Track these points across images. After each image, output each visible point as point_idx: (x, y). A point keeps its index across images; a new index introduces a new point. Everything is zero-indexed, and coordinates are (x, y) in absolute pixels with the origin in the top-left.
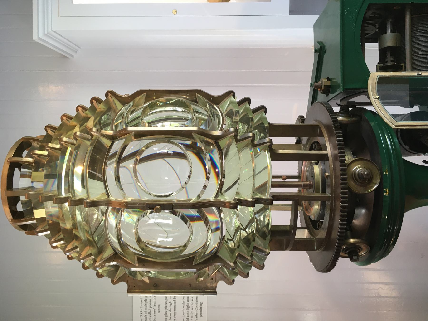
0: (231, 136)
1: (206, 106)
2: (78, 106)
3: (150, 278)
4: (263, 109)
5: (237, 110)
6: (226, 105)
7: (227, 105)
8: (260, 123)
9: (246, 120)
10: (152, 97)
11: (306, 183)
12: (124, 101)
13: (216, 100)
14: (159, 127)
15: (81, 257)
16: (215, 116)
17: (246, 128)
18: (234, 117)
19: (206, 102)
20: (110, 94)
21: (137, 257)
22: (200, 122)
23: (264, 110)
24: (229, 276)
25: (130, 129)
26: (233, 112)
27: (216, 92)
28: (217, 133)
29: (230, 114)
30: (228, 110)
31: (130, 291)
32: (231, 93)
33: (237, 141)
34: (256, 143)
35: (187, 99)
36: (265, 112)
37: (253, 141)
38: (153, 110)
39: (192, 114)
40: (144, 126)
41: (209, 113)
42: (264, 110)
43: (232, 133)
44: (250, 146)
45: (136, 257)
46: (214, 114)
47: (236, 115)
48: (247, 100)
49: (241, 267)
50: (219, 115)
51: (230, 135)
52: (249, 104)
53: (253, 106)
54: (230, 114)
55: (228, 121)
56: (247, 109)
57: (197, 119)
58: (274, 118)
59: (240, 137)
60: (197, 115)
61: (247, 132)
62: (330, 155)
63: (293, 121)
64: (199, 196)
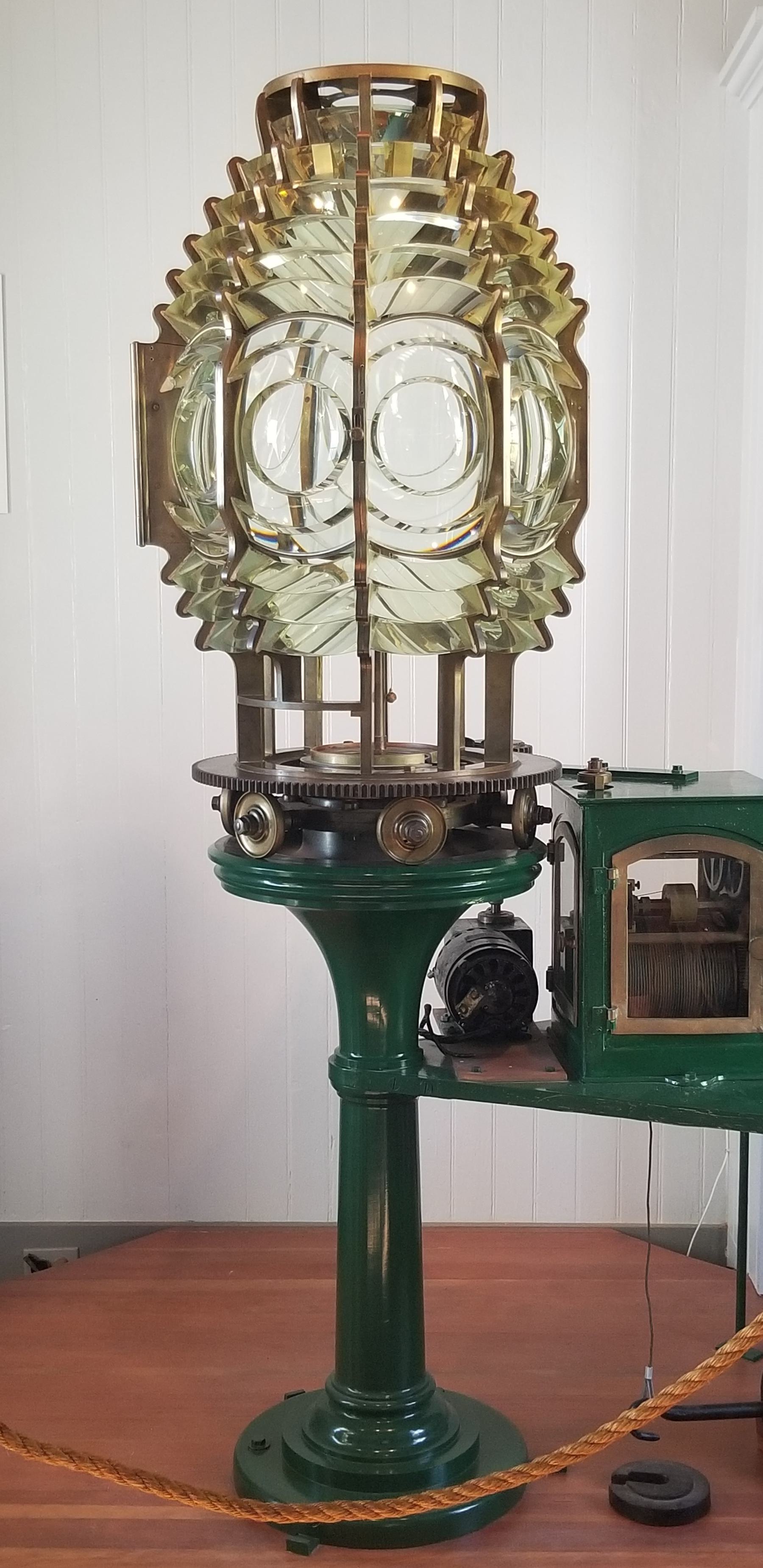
0: (490, 573)
1: (552, 521)
2: (555, 234)
3: (176, 392)
4: (547, 642)
5: (544, 586)
6: (555, 563)
7: (555, 567)
8: (516, 638)
9: (524, 604)
10: (574, 401)
11: (383, 744)
12: (567, 338)
13: (565, 544)
14: (510, 418)
15: (238, 258)
16: (531, 541)
17: (509, 605)
18: (530, 580)
19: (560, 522)
20: (580, 307)
21: (241, 380)
22: (519, 509)
23: (544, 645)
24: (182, 573)
25: (507, 368)
26: (540, 578)
27: (582, 543)
28: (497, 546)
29: (535, 571)
30: (543, 569)
31: (141, 348)
32: (579, 574)
33: (481, 586)
34: (475, 624)
35: (569, 477)
36: (539, 649)
37: (481, 617)
38: (545, 405)
39: (535, 492)
40: (515, 391)
41: (537, 529)
42: (544, 645)
43: (499, 575)
44: (466, 613)
45: (241, 376)
46: (535, 539)
47: (533, 584)
48: (565, 609)
49: (203, 600)
50: (532, 550)
51: (493, 571)
52: (557, 614)
53: (551, 622)
54: (535, 571)
55: (520, 567)
56: (545, 608)
57: (524, 502)
58: (527, 666)
59: (490, 592)
60: (531, 504)
61: (499, 606)
62: (452, 773)
63: (518, 735)
64: (374, 510)
